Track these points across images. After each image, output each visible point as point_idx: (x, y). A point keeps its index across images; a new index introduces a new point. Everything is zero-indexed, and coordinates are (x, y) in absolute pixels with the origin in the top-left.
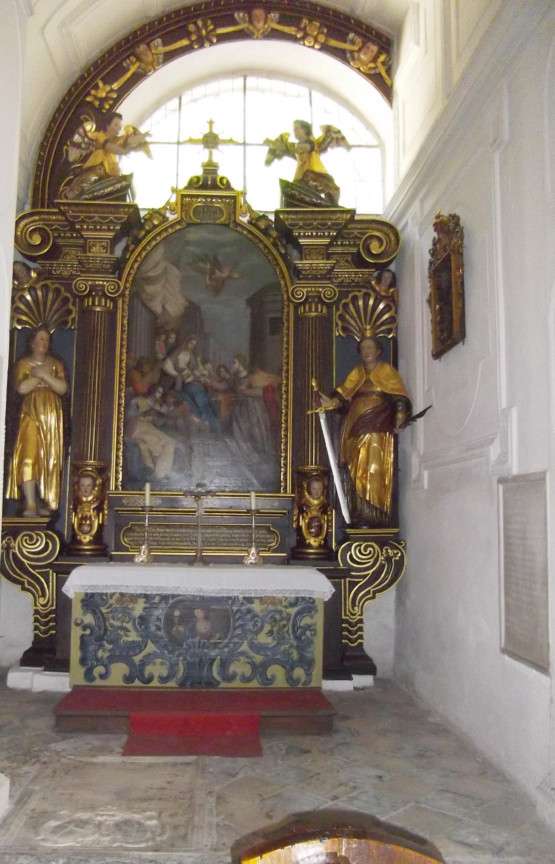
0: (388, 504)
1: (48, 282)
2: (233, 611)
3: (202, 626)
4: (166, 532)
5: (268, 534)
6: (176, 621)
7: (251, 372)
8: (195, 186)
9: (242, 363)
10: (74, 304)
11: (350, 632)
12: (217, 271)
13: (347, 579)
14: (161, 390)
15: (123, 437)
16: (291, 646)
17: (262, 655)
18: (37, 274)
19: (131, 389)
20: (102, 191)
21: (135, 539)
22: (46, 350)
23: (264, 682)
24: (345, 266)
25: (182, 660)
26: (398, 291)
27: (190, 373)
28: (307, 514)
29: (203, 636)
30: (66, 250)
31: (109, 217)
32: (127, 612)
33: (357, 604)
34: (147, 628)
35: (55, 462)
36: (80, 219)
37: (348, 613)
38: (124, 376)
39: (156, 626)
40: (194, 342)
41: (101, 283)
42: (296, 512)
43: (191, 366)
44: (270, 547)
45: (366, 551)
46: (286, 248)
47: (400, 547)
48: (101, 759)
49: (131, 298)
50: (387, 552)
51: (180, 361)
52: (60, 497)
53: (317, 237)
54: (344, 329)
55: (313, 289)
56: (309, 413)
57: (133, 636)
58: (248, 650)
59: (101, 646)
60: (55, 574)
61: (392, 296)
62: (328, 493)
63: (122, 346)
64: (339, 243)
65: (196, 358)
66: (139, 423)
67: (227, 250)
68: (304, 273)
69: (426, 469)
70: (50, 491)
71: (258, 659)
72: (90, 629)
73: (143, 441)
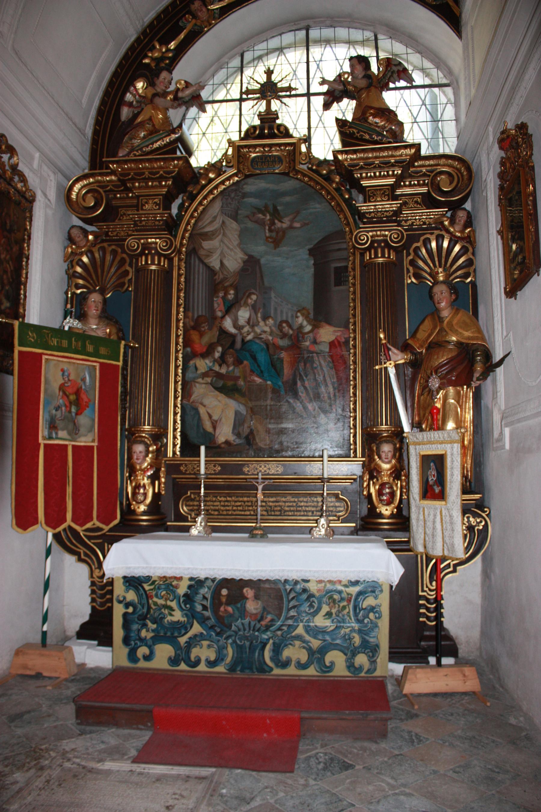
0: (469, 466)
1: (105, 245)
2: (286, 590)
3: (252, 606)
4: (227, 501)
5: (337, 502)
6: (224, 600)
7: (316, 327)
8: (253, 136)
9: (306, 317)
10: (131, 265)
12: (276, 221)
14: (220, 349)
15: (181, 400)
16: (353, 630)
19: (189, 349)
22: (99, 312)
23: (321, 669)
26: (473, 231)
27: (250, 330)
28: (377, 480)
29: (253, 616)
30: (122, 211)
34: (192, 609)
37: (425, 589)
41: (153, 240)
42: (367, 477)
43: (251, 323)
44: (339, 517)
46: (350, 194)
47: (484, 515)
48: (108, 765)
49: (188, 254)
50: (469, 521)
51: (240, 318)
53: (381, 177)
55: (379, 233)
56: (377, 367)
57: (178, 616)
58: (304, 634)
59: (145, 625)
61: (469, 237)
62: (401, 455)
64: (407, 183)
65: (256, 314)
66: (197, 385)
67: (288, 199)
68: (368, 216)
69: (506, 426)
71: (315, 644)
73: (202, 404)
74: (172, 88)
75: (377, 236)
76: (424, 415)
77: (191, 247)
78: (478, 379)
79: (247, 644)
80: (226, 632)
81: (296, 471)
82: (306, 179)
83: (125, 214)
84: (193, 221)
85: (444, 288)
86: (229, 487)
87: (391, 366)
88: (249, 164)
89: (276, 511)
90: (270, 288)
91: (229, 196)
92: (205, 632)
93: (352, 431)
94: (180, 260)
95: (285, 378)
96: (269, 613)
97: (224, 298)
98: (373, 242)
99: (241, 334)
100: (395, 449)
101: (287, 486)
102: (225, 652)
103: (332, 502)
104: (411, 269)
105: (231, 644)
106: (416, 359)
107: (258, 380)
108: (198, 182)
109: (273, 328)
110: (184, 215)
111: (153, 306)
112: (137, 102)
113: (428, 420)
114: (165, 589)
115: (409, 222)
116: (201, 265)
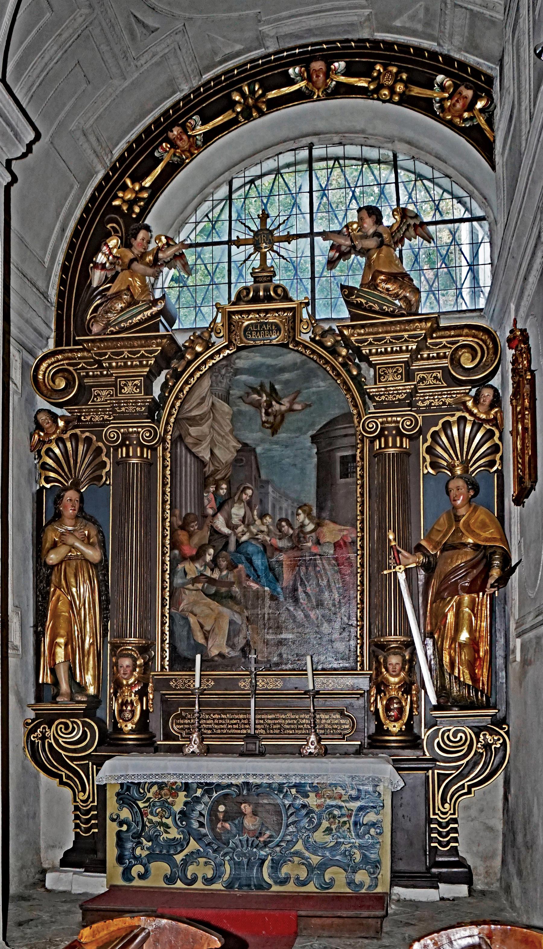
1: (77, 431)
4: (222, 719)
6: (221, 816)
9: (309, 515)
10: (107, 455)
11: (440, 833)
13: (436, 771)
14: (211, 551)
15: (169, 609)
17: (319, 856)
18: (65, 422)
19: (176, 552)
20: (130, 321)
21: (186, 726)
23: (321, 886)
24: (434, 384)
25: (228, 861)
27: (245, 530)
28: (385, 695)
30: (95, 391)
31: (139, 351)
32: (166, 806)
33: (448, 801)
34: (189, 825)
35: (91, 641)
36: (107, 357)
37: (437, 811)
38: (168, 537)
39: (199, 822)
40: (249, 492)
41: (135, 429)
42: (374, 692)
43: (246, 522)
45: (456, 737)
47: (501, 732)
49: (174, 442)
51: (233, 516)
52: (99, 680)
54: (434, 465)
55: (389, 419)
56: (385, 572)
57: (174, 833)
59: (139, 843)
60: (95, 766)
63: (164, 502)
65: (252, 511)
67: (286, 376)
68: (377, 399)
70: (87, 674)
71: (315, 860)
72: (126, 824)
73: (192, 612)
74: (152, 246)
75: (388, 422)
76: (436, 624)
77: (177, 434)
78: (492, 586)
79: (245, 860)
80: (223, 848)
81: (297, 686)
82: (308, 352)
83: (99, 395)
84: (178, 404)
85: (460, 483)
86: (223, 704)
87: (401, 571)
88: (242, 333)
89: (276, 729)
90: (267, 482)
91: (219, 372)
92: (201, 850)
93: (359, 641)
94: (164, 449)
95: (284, 585)
96: (268, 829)
97: (215, 493)
98: (383, 429)
99: (235, 534)
100: (404, 661)
101: (287, 702)
102: (223, 869)
103: (336, 719)
104: (428, 457)
105: (228, 861)
106: (429, 562)
107: (255, 586)
108: (183, 357)
109: (271, 527)
110: (168, 397)
111: (135, 503)
112: (111, 264)
113: (440, 629)
114: (160, 806)
115: (427, 403)
116: (189, 456)
